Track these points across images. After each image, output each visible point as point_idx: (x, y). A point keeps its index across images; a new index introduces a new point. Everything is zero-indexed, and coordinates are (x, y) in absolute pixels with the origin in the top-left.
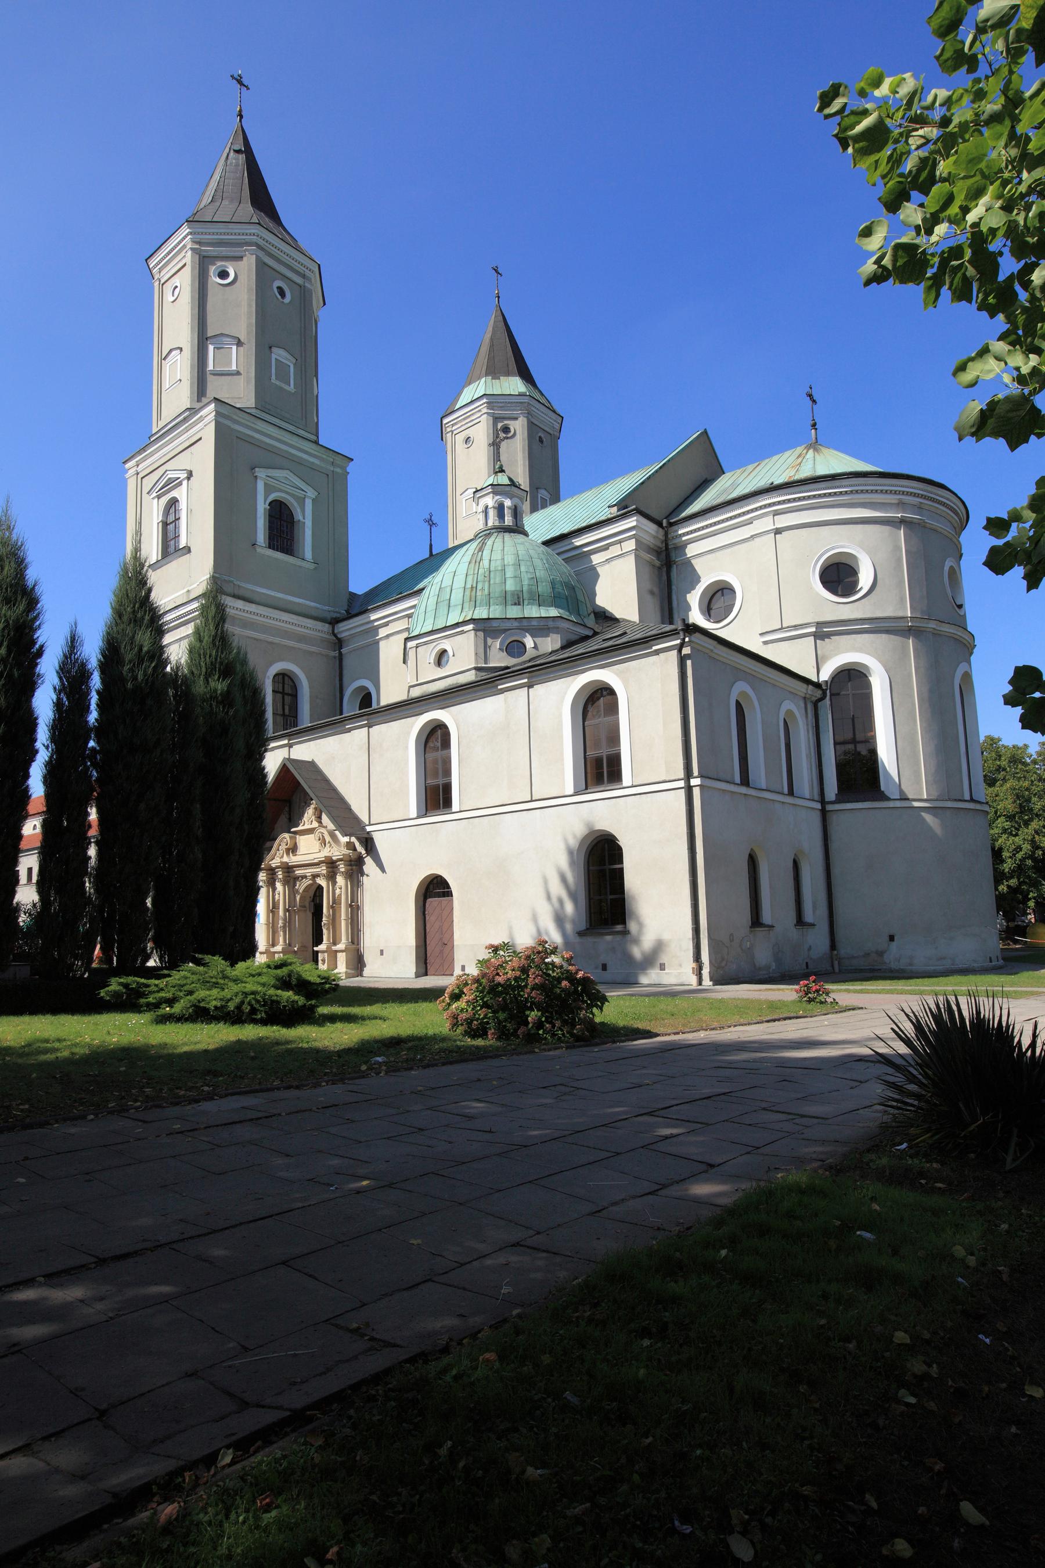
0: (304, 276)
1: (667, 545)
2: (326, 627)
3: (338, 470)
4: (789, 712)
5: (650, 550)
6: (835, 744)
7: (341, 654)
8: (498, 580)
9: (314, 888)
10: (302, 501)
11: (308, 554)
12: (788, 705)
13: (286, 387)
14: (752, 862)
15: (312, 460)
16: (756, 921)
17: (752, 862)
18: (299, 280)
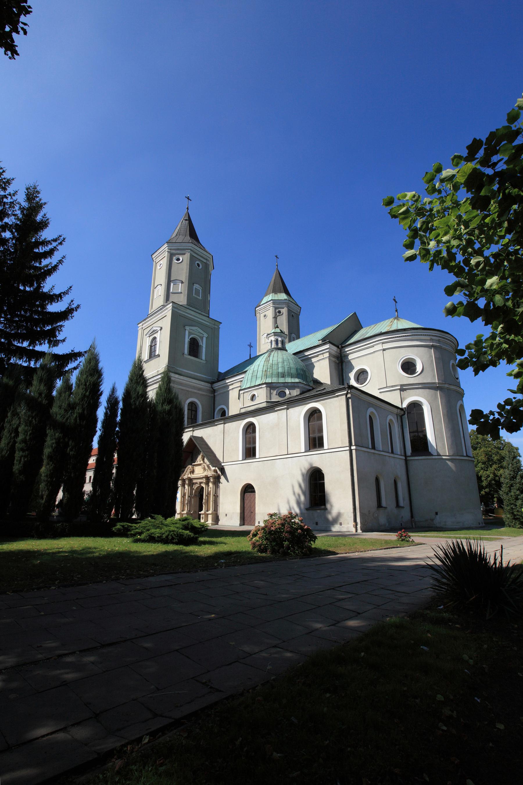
0: (207, 260)
1: (341, 355)
2: (209, 385)
3: (216, 327)
4: (391, 420)
5: (334, 357)
6: (410, 433)
7: (214, 395)
8: (275, 368)
9: (200, 488)
10: (202, 338)
11: (204, 357)
12: (390, 417)
13: (198, 297)
14: (377, 480)
15: (207, 323)
16: (379, 505)
17: (377, 480)
18: (205, 261)
